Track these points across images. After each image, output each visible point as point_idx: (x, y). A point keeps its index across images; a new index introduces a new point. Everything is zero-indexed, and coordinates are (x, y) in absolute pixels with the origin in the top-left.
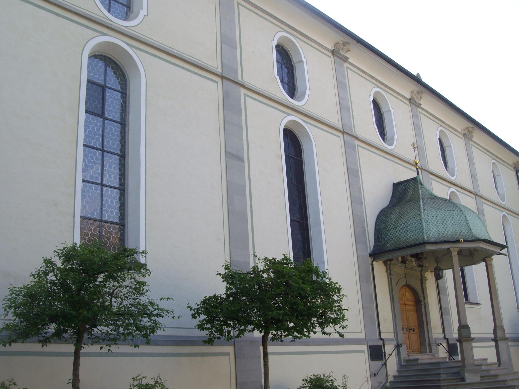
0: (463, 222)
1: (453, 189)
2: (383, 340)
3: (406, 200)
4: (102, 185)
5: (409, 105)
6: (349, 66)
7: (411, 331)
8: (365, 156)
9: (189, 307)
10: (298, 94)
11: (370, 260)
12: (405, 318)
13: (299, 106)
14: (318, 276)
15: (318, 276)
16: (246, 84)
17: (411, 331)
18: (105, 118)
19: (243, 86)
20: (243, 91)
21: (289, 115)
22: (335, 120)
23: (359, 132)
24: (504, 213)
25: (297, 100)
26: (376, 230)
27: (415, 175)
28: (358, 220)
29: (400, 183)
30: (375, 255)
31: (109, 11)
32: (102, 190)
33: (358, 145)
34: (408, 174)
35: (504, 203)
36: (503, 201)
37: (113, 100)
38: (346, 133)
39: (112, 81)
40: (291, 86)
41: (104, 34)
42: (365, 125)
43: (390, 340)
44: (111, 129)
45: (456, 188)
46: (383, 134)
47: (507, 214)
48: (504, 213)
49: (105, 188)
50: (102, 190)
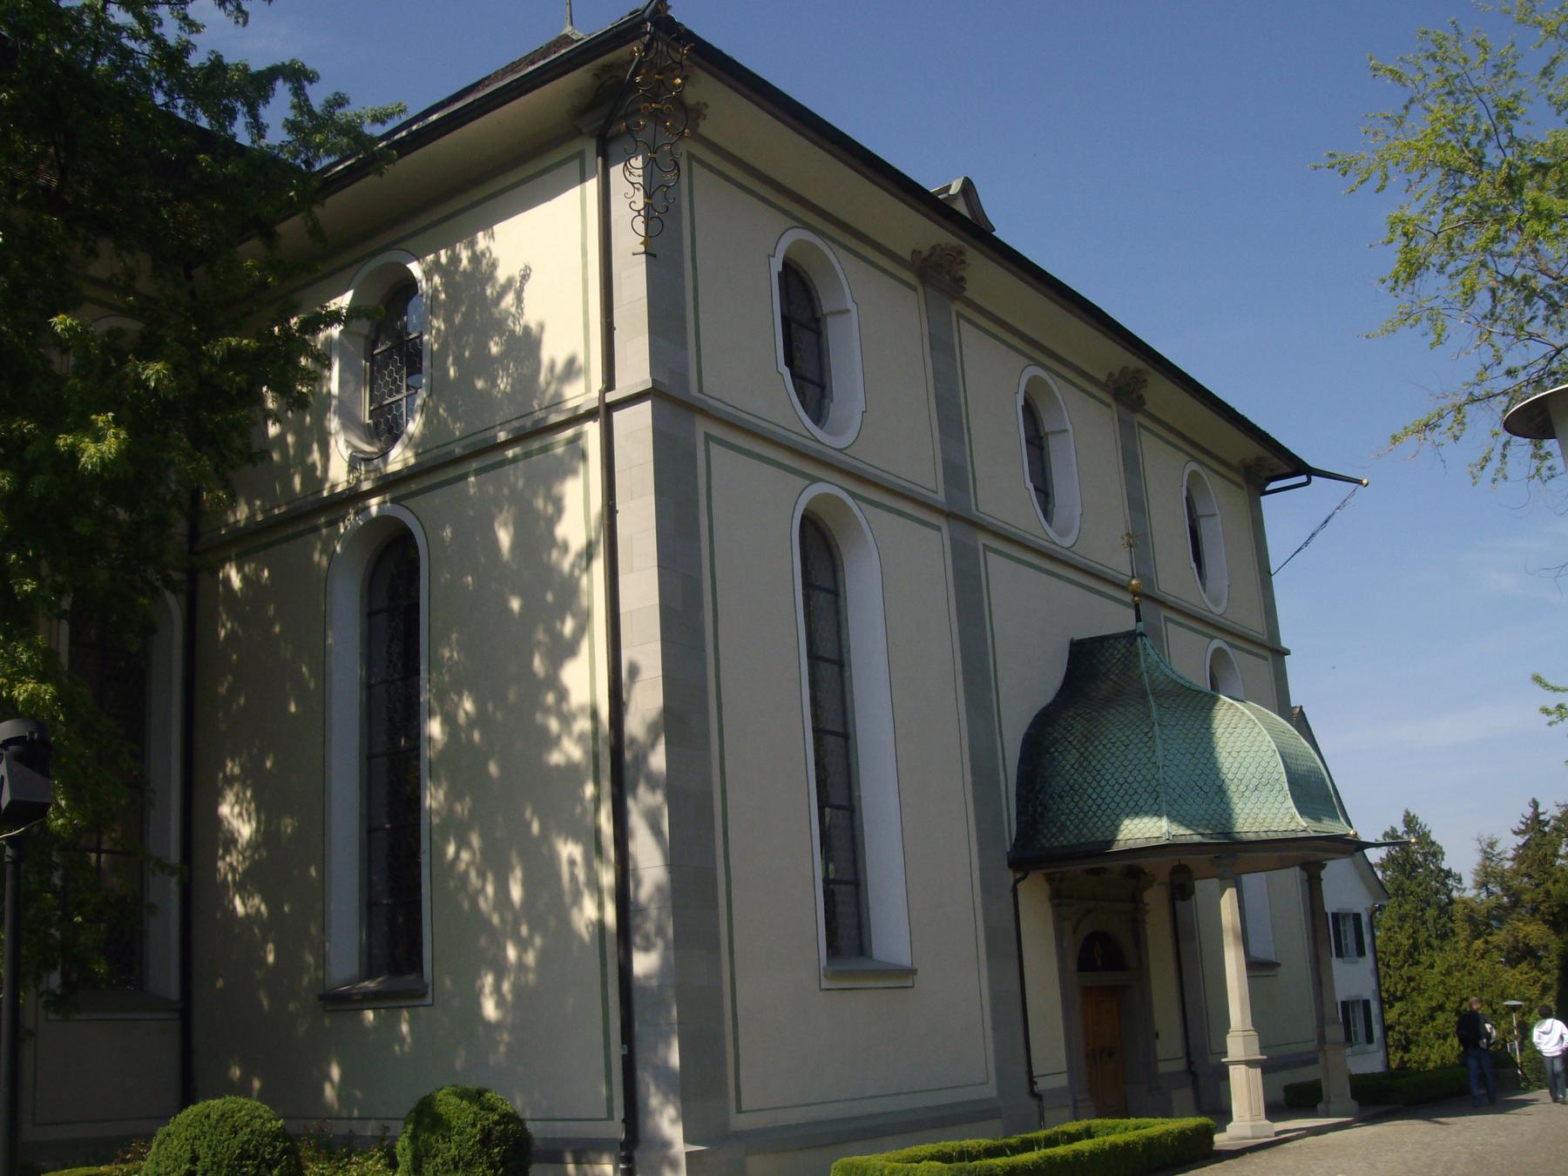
3: (319, 465)
5: (920, 289)
6: (967, 312)
8: (1006, 579)
10: (835, 410)
11: (1010, 876)
13: (840, 450)
21: (815, 480)
22: (927, 477)
24: (1217, 643)
25: (829, 433)
33: (986, 547)
34: (1114, 618)
35: (1218, 610)
36: (1217, 604)
38: (960, 517)
40: (813, 386)
42: (1003, 492)
45: (839, 479)
47: (1230, 645)
48: (1217, 643)
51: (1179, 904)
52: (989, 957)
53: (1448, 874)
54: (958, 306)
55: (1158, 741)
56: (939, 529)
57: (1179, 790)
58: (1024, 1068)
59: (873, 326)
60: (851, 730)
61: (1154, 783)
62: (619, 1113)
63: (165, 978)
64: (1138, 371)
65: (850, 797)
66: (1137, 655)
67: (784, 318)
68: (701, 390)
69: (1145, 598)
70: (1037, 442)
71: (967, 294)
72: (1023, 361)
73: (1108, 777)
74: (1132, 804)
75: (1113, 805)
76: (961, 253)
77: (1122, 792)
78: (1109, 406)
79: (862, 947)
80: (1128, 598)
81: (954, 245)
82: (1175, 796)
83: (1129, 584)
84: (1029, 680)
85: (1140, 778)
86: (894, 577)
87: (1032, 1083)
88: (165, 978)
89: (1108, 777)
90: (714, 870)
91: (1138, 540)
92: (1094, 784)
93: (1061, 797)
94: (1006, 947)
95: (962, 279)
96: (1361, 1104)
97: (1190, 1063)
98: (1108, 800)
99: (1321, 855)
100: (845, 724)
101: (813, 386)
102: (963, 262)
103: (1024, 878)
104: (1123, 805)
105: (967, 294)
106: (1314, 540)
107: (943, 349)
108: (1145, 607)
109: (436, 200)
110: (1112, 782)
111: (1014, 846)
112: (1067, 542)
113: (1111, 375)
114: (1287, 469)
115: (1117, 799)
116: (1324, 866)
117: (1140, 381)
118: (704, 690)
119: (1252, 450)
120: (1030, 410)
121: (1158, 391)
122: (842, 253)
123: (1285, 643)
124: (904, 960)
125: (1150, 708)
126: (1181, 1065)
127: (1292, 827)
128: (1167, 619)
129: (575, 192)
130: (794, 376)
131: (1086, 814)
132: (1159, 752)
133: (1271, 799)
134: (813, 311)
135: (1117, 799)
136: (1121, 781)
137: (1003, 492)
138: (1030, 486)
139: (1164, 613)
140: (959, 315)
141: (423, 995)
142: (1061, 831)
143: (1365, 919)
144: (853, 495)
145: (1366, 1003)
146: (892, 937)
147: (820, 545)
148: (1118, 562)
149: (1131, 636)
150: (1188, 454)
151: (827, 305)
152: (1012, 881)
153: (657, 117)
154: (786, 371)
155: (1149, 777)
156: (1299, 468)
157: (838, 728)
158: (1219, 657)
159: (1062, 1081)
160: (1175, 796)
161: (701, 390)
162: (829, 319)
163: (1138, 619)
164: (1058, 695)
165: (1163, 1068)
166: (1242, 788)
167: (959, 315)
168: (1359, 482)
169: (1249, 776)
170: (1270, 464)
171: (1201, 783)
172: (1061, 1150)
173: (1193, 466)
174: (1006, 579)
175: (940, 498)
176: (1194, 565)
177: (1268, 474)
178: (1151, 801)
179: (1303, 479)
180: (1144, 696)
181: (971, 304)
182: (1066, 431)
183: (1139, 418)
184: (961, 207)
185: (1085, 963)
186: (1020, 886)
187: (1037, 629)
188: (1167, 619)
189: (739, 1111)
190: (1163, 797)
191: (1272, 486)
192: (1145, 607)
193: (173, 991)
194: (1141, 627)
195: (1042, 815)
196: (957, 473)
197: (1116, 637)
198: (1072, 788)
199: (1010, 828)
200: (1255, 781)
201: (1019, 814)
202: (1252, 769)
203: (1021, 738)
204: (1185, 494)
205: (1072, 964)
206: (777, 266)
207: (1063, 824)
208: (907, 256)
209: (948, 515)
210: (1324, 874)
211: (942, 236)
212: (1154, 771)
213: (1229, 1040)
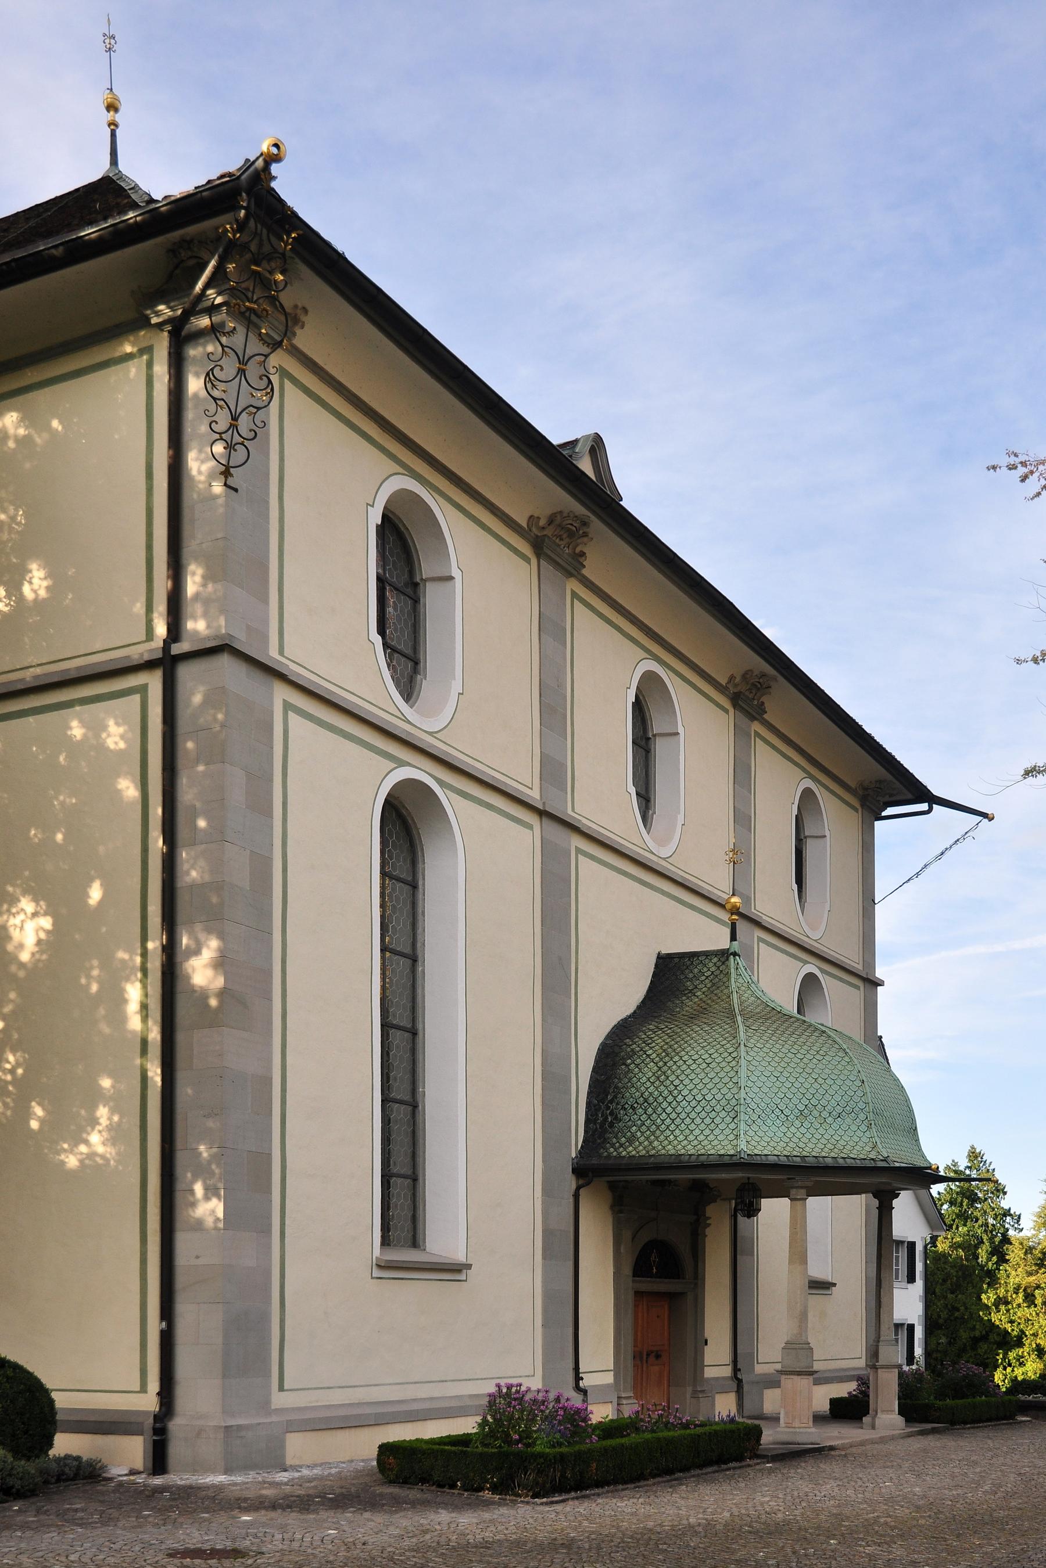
0: (856, 1099)
2: (584, 1392)
5: (534, 561)
7: (652, 1359)
8: (595, 882)
9: (988, 468)
10: (427, 687)
11: (571, 1183)
12: (560, 561)
13: (431, 734)
16: (293, 669)
17: (652, 1359)
19: (281, 677)
20: (281, 693)
21: (401, 763)
22: (523, 775)
23: (583, 808)
26: (595, 1070)
28: (554, 1080)
29: (670, 957)
33: (578, 851)
34: (705, 934)
42: (601, 793)
43: (602, 1388)
46: (645, 798)
51: (741, 1219)
52: (544, 1258)
53: (1007, 1213)
54: (572, 585)
55: (743, 1062)
56: (530, 827)
57: (758, 1111)
58: (571, 1365)
59: (482, 583)
60: (420, 1027)
61: (734, 1102)
62: (154, 1386)
64: (763, 675)
65: (414, 1091)
66: (728, 975)
67: (379, 579)
68: (281, 652)
69: (741, 918)
70: (643, 743)
71: (585, 572)
73: (685, 1092)
74: (708, 1121)
75: (688, 1121)
76: (585, 524)
77: (699, 1109)
78: (727, 711)
79: (415, 1241)
80: (725, 916)
81: (575, 512)
82: (755, 1117)
83: (728, 901)
84: (609, 992)
85: (719, 1097)
86: (480, 860)
87: (578, 1378)
89: (685, 1092)
91: (740, 858)
92: (670, 1099)
93: (634, 1108)
94: (563, 1250)
97: (736, 1370)
98: (683, 1115)
100: (414, 1020)
102: (585, 535)
103: (588, 1184)
104: (698, 1121)
105: (585, 572)
106: (927, 870)
107: (551, 630)
108: (742, 927)
110: (689, 1098)
111: (580, 1153)
112: (665, 852)
113: (732, 678)
114: (910, 796)
115: (693, 1115)
116: (897, 1196)
117: (764, 684)
118: (269, 973)
120: (639, 708)
121: (781, 701)
124: (461, 1257)
125: (737, 1029)
126: (727, 1372)
127: (873, 1155)
128: (760, 940)
129: (134, 370)
130: (386, 645)
131: (658, 1127)
132: (743, 1073)
133: (854, 1128)
134: (411, 573)
135: (693, 1115)
136: (699, 1097)
137: (601, 793)
138: (633, 790)
139: (759, 933)
140: (574, 595)
142: (631, 1141)
143: (919, 1248)
145: (911, 1328)
146: (446, 1235)
147: (404, 823)
148: (718, 879)
149: (724, 955)
150: (804, 770)
151: (427, 569)
152: (574, 1186)
154: (378, 640)
155: (729, 1096)
156: (918, 793)
157: (406, 1023)
158: (810, 983)
159: (609, 1378)
160: (755, 1117)
161: (281, 652)
162: (429, 586)
163: (733, 938)
164: (639, 1007)
165: (709, 1373)
167: (574, 595)
170: (886, 786)
171: (782, 1106)
173: (808, 783)
174: (595, 882)
175: (534, 795)
176: (795, 887)
177: (887, 799)
178: (728, 1119)
179: (924, 807)
180: (732, 1016)
183: (756, 726)
184: (586, 466)
186: (582, 1191)
187: (620, 945)
188: (760, 940)
189: (281, 1388)
190: (742, 1116)
191: (890, 811)
192: (742, 927)
195: (611, 1125)
196: (554, 770)
197: (707, 954)
198: (646, 1100)
200: (839, 1109)
203: (615, 1022)
204: (795, 812)
205: (627, 1270)
207: (633, 1135)
209: (542, 814)
211: (560, 499)
212: (735, 1090)
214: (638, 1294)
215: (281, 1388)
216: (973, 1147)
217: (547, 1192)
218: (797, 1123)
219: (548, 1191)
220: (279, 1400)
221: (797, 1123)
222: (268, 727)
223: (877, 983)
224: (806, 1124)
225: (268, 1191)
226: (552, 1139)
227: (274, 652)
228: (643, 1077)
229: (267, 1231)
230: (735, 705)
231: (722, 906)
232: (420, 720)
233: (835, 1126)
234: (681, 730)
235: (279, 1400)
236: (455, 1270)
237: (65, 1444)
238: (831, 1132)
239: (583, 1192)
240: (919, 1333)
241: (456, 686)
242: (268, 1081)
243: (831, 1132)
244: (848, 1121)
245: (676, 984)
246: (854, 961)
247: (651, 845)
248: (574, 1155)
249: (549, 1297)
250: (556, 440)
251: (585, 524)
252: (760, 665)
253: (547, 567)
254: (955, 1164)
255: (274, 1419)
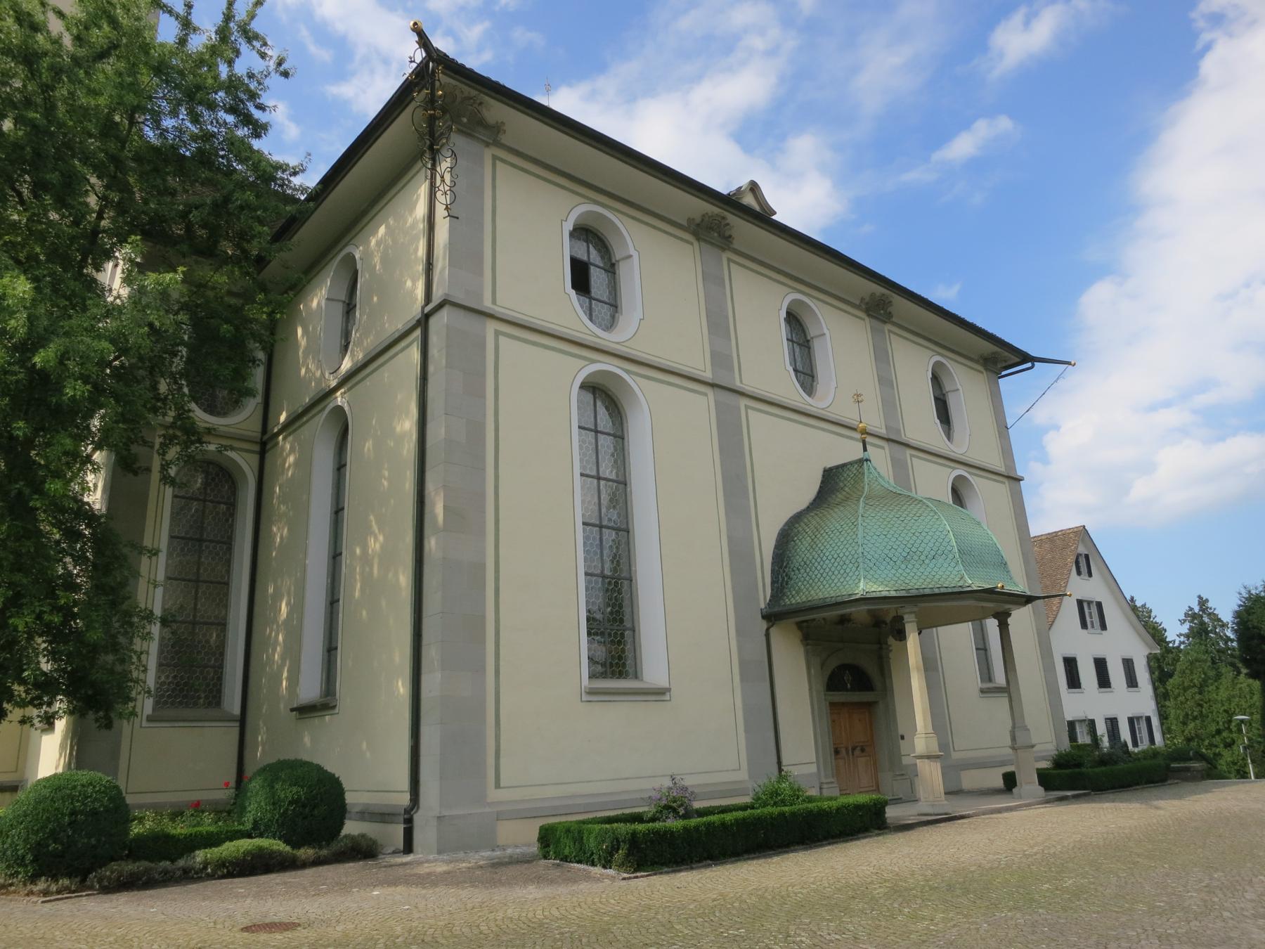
1: (961, 471)
4: (597, 432)
10: (820, 388)
11: (764, 625)
14: (194, 96)
15: (194, 96)
17: (857, 752)
18: (591, 298)
19: (491, 316)
22: (699, 362)
27: (859, 454)
28: (739, 553)
29: (831, 469)
30: (772, 617)
31: (591, 320)
32: (601, 534)
37: (597, 278)
39: (595, 257)
40: (807, 376)
41: (593, 361)
44: (600, 312)
49: (594, 473)
50: (601, 534)
52: (742, 680)
54: (729, 254)
63: (232, 702)
72: (931, 353)
80: (858, 436)
88: (232, 702)
90: (484, 617)
95: (730, 236)
96: (1046, 790)
99: (1007, 606)
101: (807, 376)
109: (364, 213)
113: (862, 299)
114: (1018, 360)
116: (1010, 615)
118: (482, 496)
119: (989, 348)
120: (936, 379)
122: (625, 219)
123: (1020, 473)
124: (663, 683)
133: (946, 565)
134: (610, 259)
141: (334, 707)
142: (798, 593)
144: (627, 371)
145: (1148, 719)
149: (861, 462)
153: (467, 133)
159: (813, 769)
163: (865, 449)
166: (923, 557)
167: (890, 331)
168: (1068, 363)
169: (928, 549)
170: (1002, 358)
171: (890, 555)
172: (713, 818)
174: (762, 429)
175: (708, 375)
179: (1029, 365)
181: (895, 324)
182: (631, 256)
184: (749, 200)
185: (834, 683)
188: (912, 456)
189: (498, 786)
193: (237, 710)
194: (866, 455)
196: (721, 359)
197: (851, 463)
199: (764, 594)
200: (933, 553)
201: (773, 583)
202: (931, 545)
206: (783, 314)
208: (685, 223)
210: (1009, 620)
213: (916, 741)
214: (833, 705)
215: (498, 786)
216: (1200, 597)
217: (740, 632)
218: (903, 566)
219: (742, 632)
220: (494, 795)
221: (903, 566)
222: (482, 346)
223: (1018, 480)
224: (910, 566)
225: (483, 642)
226: (741, 592)
227: (738, 383)
228: (802, 548)
229: (481, 669)
230: (869, 315)
231: (854, 429)
232: (958, 449)
233: (931, 565)
234: (826, 331)
235: (494, 795)
236: (660, 693)
237: (351, 828)
238: (929, 570)
239: (772, 630)
240: (1155, 722)
241: (834, 384)
242: (482, 567)
243: (929, 570)
244: (941, 560)
245: (833, 484)
246: (997, 463)
247: (952, 447)
248: (763, 606)
249: (748, 711)
250: (725, 192)
251: (724, 218)
252: (879, 290)
253: (705, 246)
254: (1191, 609)
255: (487, 810)
